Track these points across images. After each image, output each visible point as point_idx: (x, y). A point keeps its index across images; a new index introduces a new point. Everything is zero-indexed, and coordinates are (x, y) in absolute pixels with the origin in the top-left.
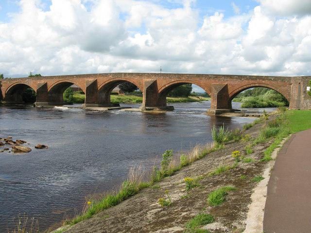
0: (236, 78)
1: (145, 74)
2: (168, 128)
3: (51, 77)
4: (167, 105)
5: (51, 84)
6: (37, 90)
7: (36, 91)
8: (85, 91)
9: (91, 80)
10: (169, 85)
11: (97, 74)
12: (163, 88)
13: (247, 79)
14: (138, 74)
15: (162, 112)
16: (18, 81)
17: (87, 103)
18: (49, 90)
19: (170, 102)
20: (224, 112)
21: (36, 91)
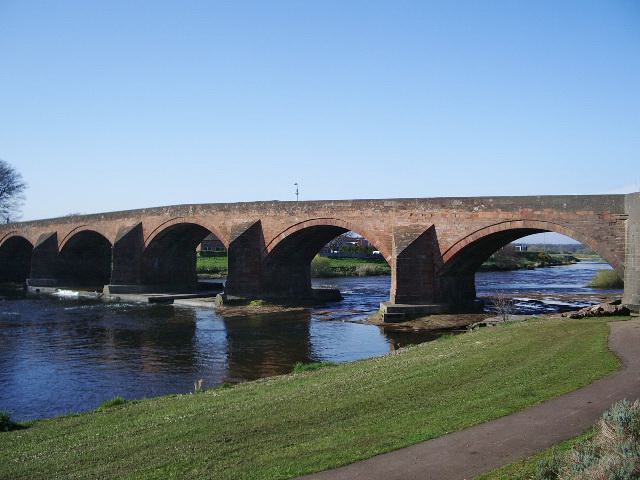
0: (458, 207)
1: (252, 203)
2: (311, 365)
3: (150, 211)
4: (315, 286)
5: (275, 230)
6: (116, 244)
7: (113, 243)
8: (392, 258)
9: (130, 223)
10: (288, 233)
11: (141, 210)
12: (153, 236)
13: (489, 208)
14: (358, 204)
15: (397, 325)
16: (12, 230)
17: (231, 288)
18: (147, 245)
19: (327, 275)
20: (421, 313)
21: (113, 243)
